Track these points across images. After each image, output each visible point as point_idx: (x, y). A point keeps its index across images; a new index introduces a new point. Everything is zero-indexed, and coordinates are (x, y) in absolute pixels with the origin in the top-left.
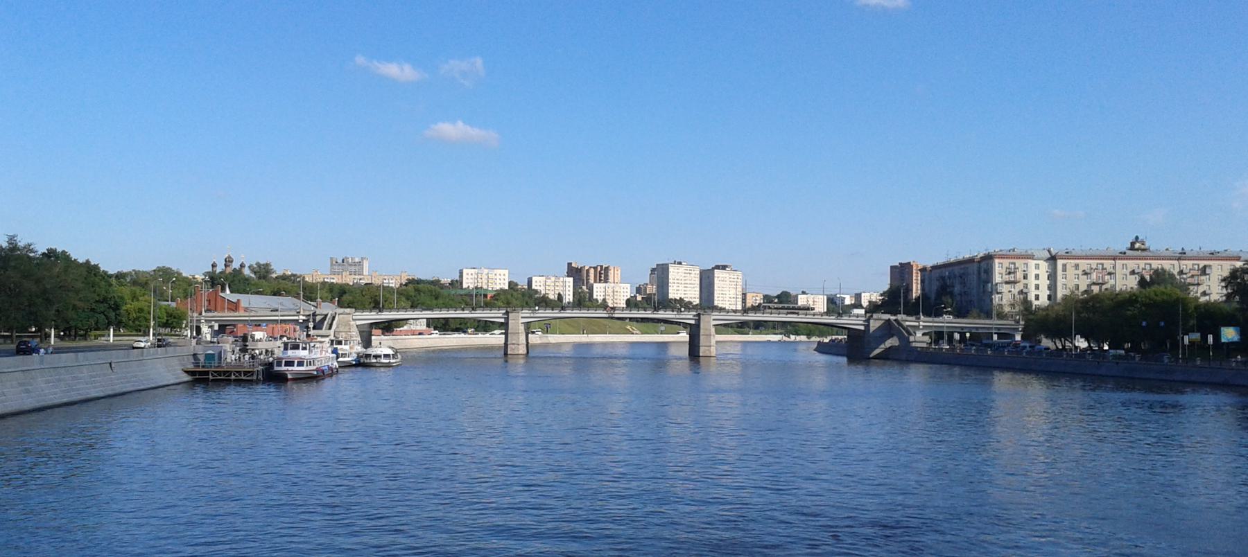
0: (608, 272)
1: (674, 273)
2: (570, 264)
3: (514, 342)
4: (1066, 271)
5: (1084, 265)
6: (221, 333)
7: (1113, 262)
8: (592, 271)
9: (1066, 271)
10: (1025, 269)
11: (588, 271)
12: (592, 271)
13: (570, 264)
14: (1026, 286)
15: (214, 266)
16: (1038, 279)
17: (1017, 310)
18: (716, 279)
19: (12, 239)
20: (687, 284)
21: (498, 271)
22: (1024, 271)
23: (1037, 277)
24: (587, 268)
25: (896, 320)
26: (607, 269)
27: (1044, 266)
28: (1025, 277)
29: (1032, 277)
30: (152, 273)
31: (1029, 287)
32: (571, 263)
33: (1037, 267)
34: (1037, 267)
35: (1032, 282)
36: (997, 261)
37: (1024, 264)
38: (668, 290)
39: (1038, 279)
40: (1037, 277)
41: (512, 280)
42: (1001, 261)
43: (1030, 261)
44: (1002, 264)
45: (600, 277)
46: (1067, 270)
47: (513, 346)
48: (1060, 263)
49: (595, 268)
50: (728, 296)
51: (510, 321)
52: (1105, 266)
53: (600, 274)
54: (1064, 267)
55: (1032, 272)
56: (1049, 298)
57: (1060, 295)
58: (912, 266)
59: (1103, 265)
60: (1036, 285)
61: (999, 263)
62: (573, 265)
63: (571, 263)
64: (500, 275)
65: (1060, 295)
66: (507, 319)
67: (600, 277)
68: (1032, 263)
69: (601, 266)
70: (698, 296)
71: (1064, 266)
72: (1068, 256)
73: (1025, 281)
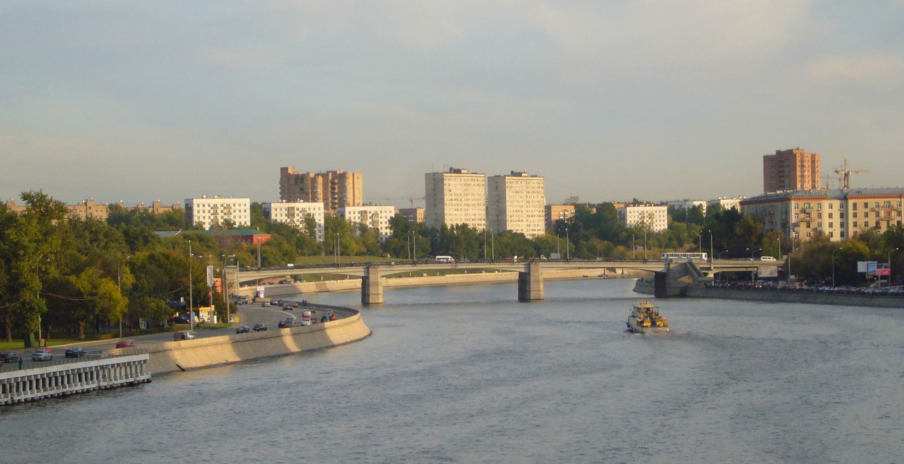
0: (344, 182)
1: (452, 185)
2: (284, 170)
3: (374, 293)
4: (856, 210)
5: (872, 203)
6: (452, 256)
7: (899, 200)
8: (320, 180)
9: (856, 210)
10: (819, 209)
11: (314, 180)
12: (320, 180)
13: (284, 170)
14: (820, 225)
15: (66, 203)
16: (832, 218)
17: (209, 283)
18: (507, 190)
19: (41, 190)
20: (468, 200)
21: (383, 207)
22: (818, 210)
23: (830, 216)
24: (312, 175)
25: (152, 257)
26: (343, 177)
27: (837, 204)
28: (820, 216)
29: (825, 216)
30: (307, 226)
31: (822, 225)
32: (287, 169)
33: (831, 207)
34: (831, 207)
35: (826, 220)
36: (793, 203)
37: (818, 204)
38: (443, 208)
39: (832, 218)
40: (830, 216)
41: (255, 200)
42: (797, 202)
43: (823, 201)
44: (798, 204)
45: (333, 189)
46: (858, 209)
47: (374, 297)
48: (851, 202)
49: (325, 176)
50: (525, 213)
51: (370, 275)
52: (892, 204)
53: (333, 184)
54: (855, 205)
55: (826, 211)
56: (842, 235)
57: (851, 230)
58: (795, 156)
59: (889, 202)
60: (829, 223)
61: (795, 204)
62: (290, 171)
63: (287, 169)
64: (386, 212)
65: (851, 230)
66: (368, 272)
67: (333, 189)
68: (825, 203)
69: (334, 173)
70: (484, 217)
71: (855, 205)
72: (859, 194)
73: (820, 221)
